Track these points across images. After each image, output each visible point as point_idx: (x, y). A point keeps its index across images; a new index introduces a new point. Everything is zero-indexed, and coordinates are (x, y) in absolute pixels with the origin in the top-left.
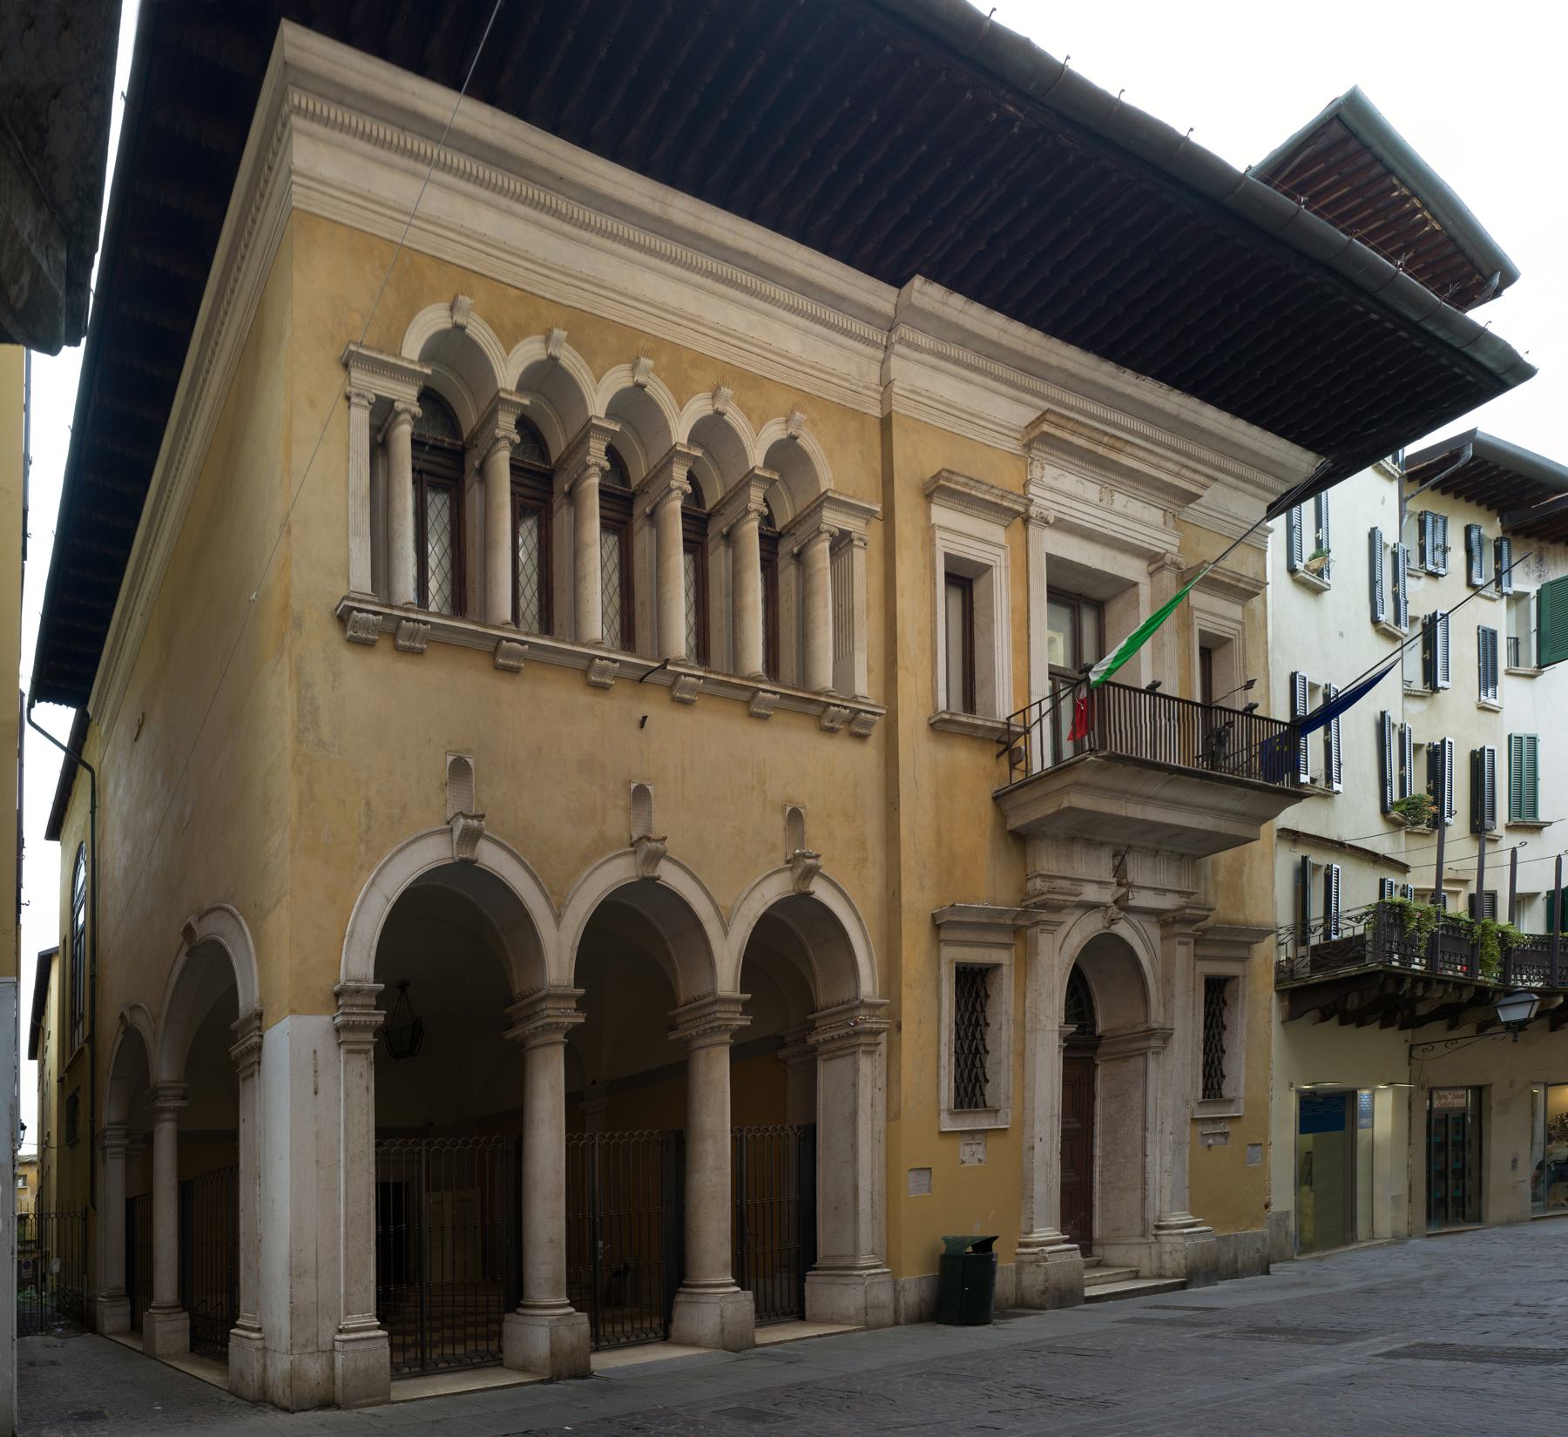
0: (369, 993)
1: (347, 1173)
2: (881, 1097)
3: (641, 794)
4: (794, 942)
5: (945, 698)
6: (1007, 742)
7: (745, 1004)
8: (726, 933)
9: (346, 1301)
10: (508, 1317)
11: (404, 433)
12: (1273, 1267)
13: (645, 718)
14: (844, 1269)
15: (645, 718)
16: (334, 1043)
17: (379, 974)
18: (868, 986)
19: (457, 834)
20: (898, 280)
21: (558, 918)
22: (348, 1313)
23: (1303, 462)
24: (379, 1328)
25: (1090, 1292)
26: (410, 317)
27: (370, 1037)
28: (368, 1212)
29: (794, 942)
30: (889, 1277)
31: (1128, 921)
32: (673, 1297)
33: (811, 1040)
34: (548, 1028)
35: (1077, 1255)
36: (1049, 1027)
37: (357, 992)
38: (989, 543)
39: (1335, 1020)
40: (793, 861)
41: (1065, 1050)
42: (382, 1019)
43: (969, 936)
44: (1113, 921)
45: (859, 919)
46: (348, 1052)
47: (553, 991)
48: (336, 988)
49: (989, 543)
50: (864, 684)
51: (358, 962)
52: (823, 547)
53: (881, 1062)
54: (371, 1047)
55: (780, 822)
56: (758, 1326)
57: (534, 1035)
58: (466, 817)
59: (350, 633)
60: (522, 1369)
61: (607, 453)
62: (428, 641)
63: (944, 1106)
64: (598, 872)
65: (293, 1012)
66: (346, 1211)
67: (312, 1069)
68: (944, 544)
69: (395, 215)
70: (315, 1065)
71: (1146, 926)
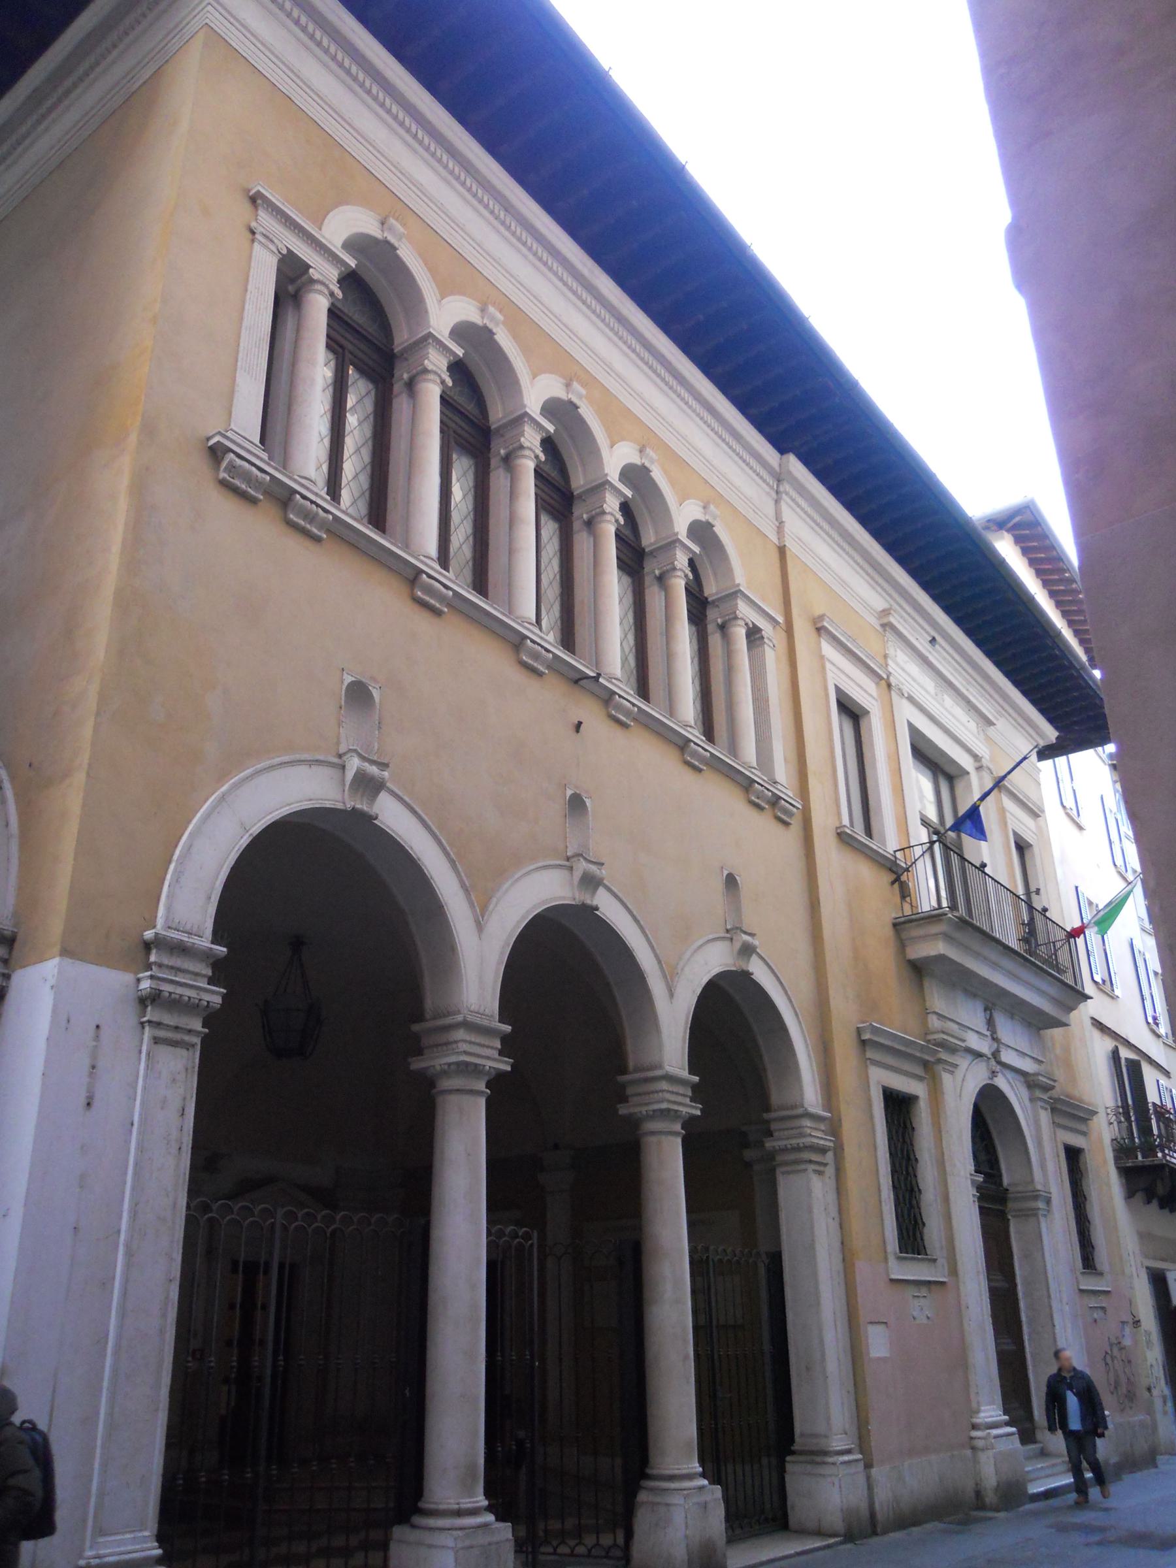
0: (205, 956)
1: (129, 1254)
2: (834, 1225)
3: (576, 804)
4: (732, 1020)
5: (848, 816)
6: (897, 874)
7: (505, 1039)
8: (671, 995)
9: (99, 1506)
10: (398, 1531)
11: (318, 307)
12: (1160, 1459)
13: (580, 723)
14: (818, 1455)
15: (580, 723)
16: (133, 1021)
17: (505, 1012)
18: (811, 1095)
19: (350, 775)
20: (782, 451)
21: (480, 927)
22: (101, 1531)
23: (1051, 734)
24: (1007, 1424)
25: (1035, 1488)
26: (337, 207)
27: (197, 1025)
28: (162, 1332)
29: (732, 1020)
30: (861, 1464)
31: (1004, 1075)
32: (634, 1495)
33: (769, 1144)
34: (666, 1114)
35: (1016, 1441)
36: (962, 1173)
37: (181, 949)
38: (866, 691)
39: (1155, 1203)
40: (730, 933)
41: (980, 1199)
42: (217, 1000)
43: (890, 1060)
44: (994, 1073)
45: (797, 1015)
46: (156, 1041)
47: (470, 1018)
48: (149, 934)
49: (866, 691)
50: (783, 772)
51: (189, 901)
52: (740, 632)
53: (831, 1183)
54: (197, 1040)
55: (719, 884)
56: (730, 1541)
57: (445, 1073)
58: (363, 758)
59: (223, 475)
60: (819, 1533)
61: (621, 510)
62: (328, 531)
63: (890, 1249)
64: (263, 779)
65: (65, 952)
66: (121, 1326)
67: (87, 1062)
68: (833, 678)
69: (326, 107)
70: (94, 1054)
71: (1018, 1084)
